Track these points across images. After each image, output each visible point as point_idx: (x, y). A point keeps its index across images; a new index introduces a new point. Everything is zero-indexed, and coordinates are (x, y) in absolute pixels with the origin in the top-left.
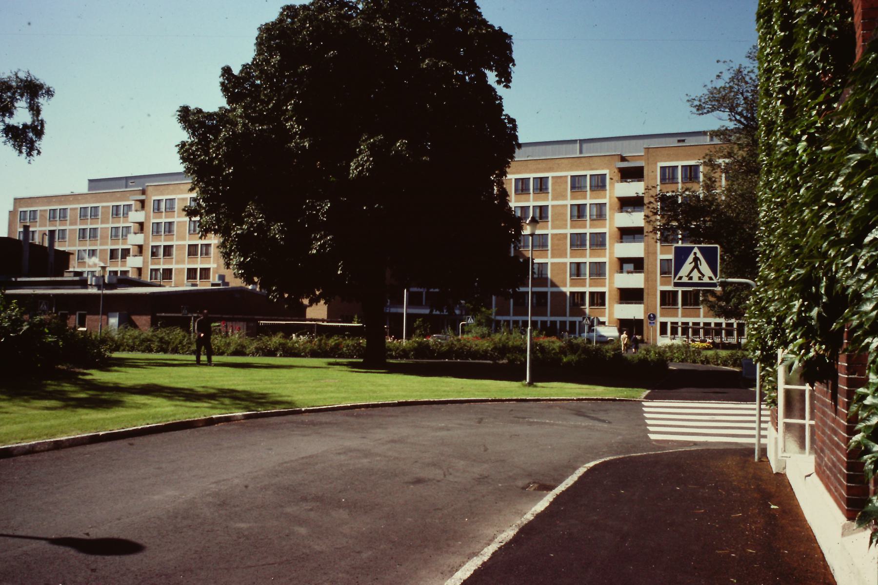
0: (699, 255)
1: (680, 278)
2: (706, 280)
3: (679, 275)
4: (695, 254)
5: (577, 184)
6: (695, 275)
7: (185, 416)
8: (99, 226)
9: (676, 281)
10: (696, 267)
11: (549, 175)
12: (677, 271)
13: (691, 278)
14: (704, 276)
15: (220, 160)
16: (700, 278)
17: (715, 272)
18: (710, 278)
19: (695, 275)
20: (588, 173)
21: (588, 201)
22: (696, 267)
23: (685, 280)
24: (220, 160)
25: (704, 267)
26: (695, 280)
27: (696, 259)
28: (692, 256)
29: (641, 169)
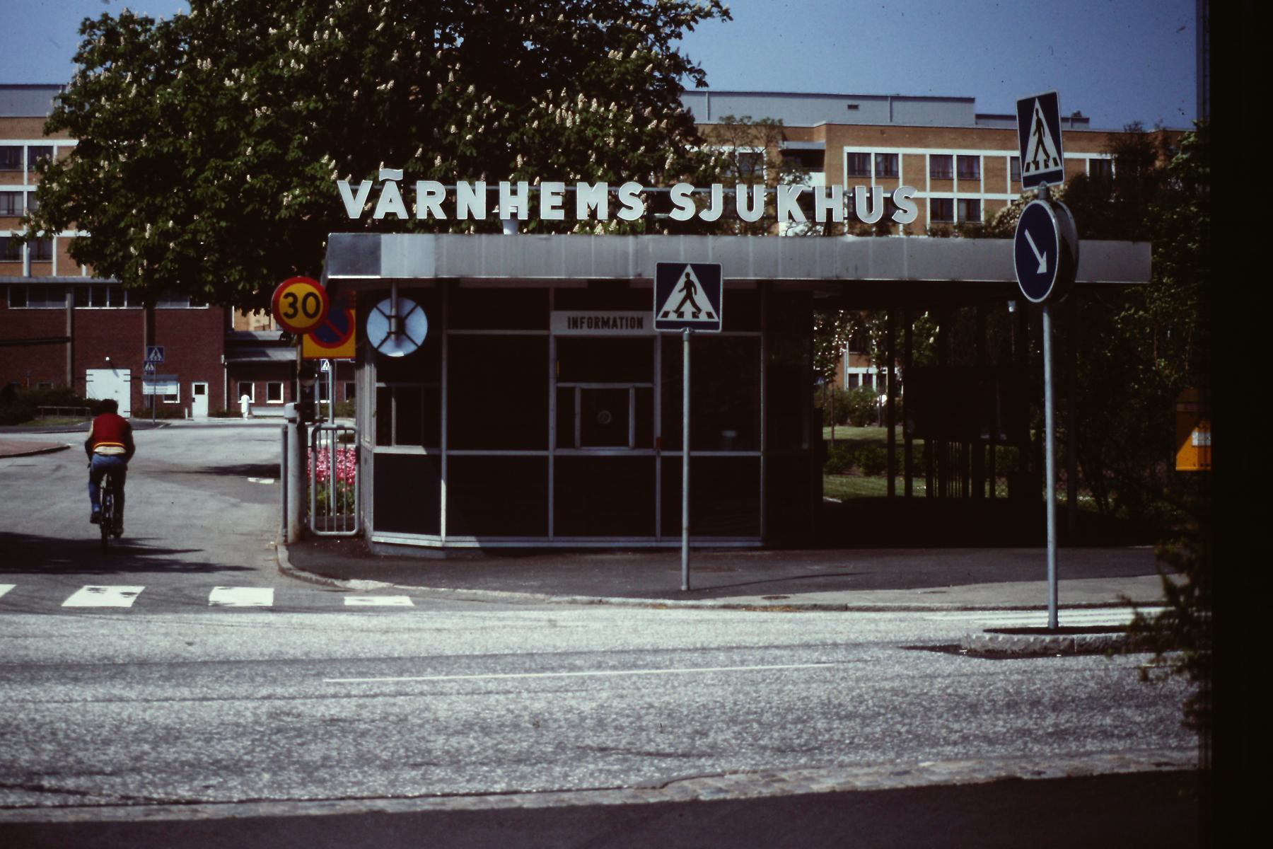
0: (693, 278)
1: (666, 314)
2: (703, 317)
3: (666, 308)
4: (688, 275)
5: (858, 165)
6: (688, 309)
7: (649, 771)
8: (982, 196)
9: (659, 318)
10: (689, 297)
11: (982, 153)
12: (661, 304)
13: (681, 315)
14: (699, 310)
15: (192, 38)
16: (694, 315)
17: (715, 304)
18: (709, 315)
19: (688, 309)
20: (955, 152)
21: (955, 195)
22: (689, 297)
23: (673, 317)
24: (192, 38)
25: (701, 298)
26: (688, 317)
27: (689, 285)
28: (683, 280)
29: (820, 154)
